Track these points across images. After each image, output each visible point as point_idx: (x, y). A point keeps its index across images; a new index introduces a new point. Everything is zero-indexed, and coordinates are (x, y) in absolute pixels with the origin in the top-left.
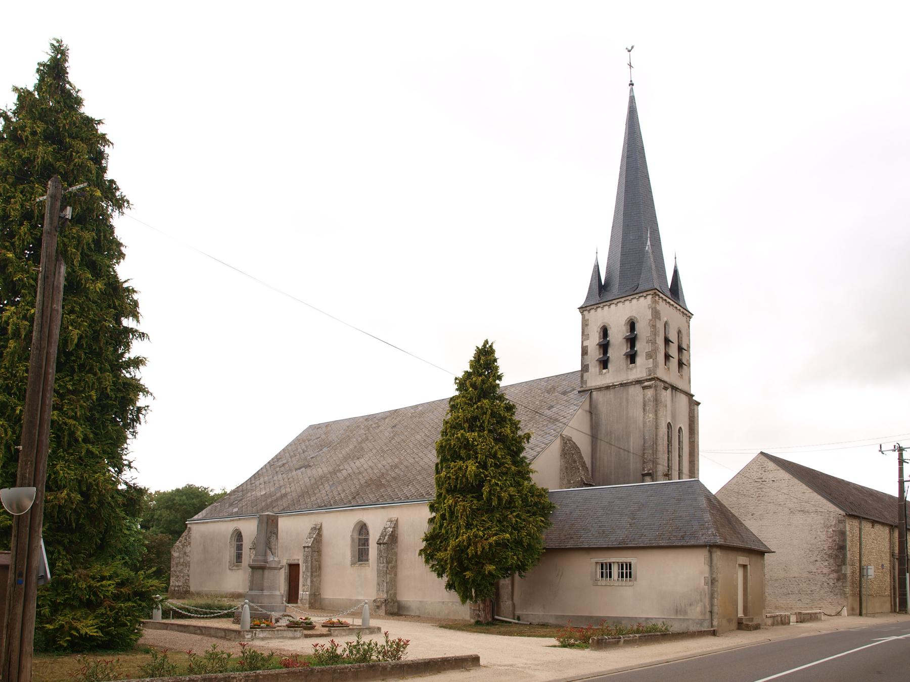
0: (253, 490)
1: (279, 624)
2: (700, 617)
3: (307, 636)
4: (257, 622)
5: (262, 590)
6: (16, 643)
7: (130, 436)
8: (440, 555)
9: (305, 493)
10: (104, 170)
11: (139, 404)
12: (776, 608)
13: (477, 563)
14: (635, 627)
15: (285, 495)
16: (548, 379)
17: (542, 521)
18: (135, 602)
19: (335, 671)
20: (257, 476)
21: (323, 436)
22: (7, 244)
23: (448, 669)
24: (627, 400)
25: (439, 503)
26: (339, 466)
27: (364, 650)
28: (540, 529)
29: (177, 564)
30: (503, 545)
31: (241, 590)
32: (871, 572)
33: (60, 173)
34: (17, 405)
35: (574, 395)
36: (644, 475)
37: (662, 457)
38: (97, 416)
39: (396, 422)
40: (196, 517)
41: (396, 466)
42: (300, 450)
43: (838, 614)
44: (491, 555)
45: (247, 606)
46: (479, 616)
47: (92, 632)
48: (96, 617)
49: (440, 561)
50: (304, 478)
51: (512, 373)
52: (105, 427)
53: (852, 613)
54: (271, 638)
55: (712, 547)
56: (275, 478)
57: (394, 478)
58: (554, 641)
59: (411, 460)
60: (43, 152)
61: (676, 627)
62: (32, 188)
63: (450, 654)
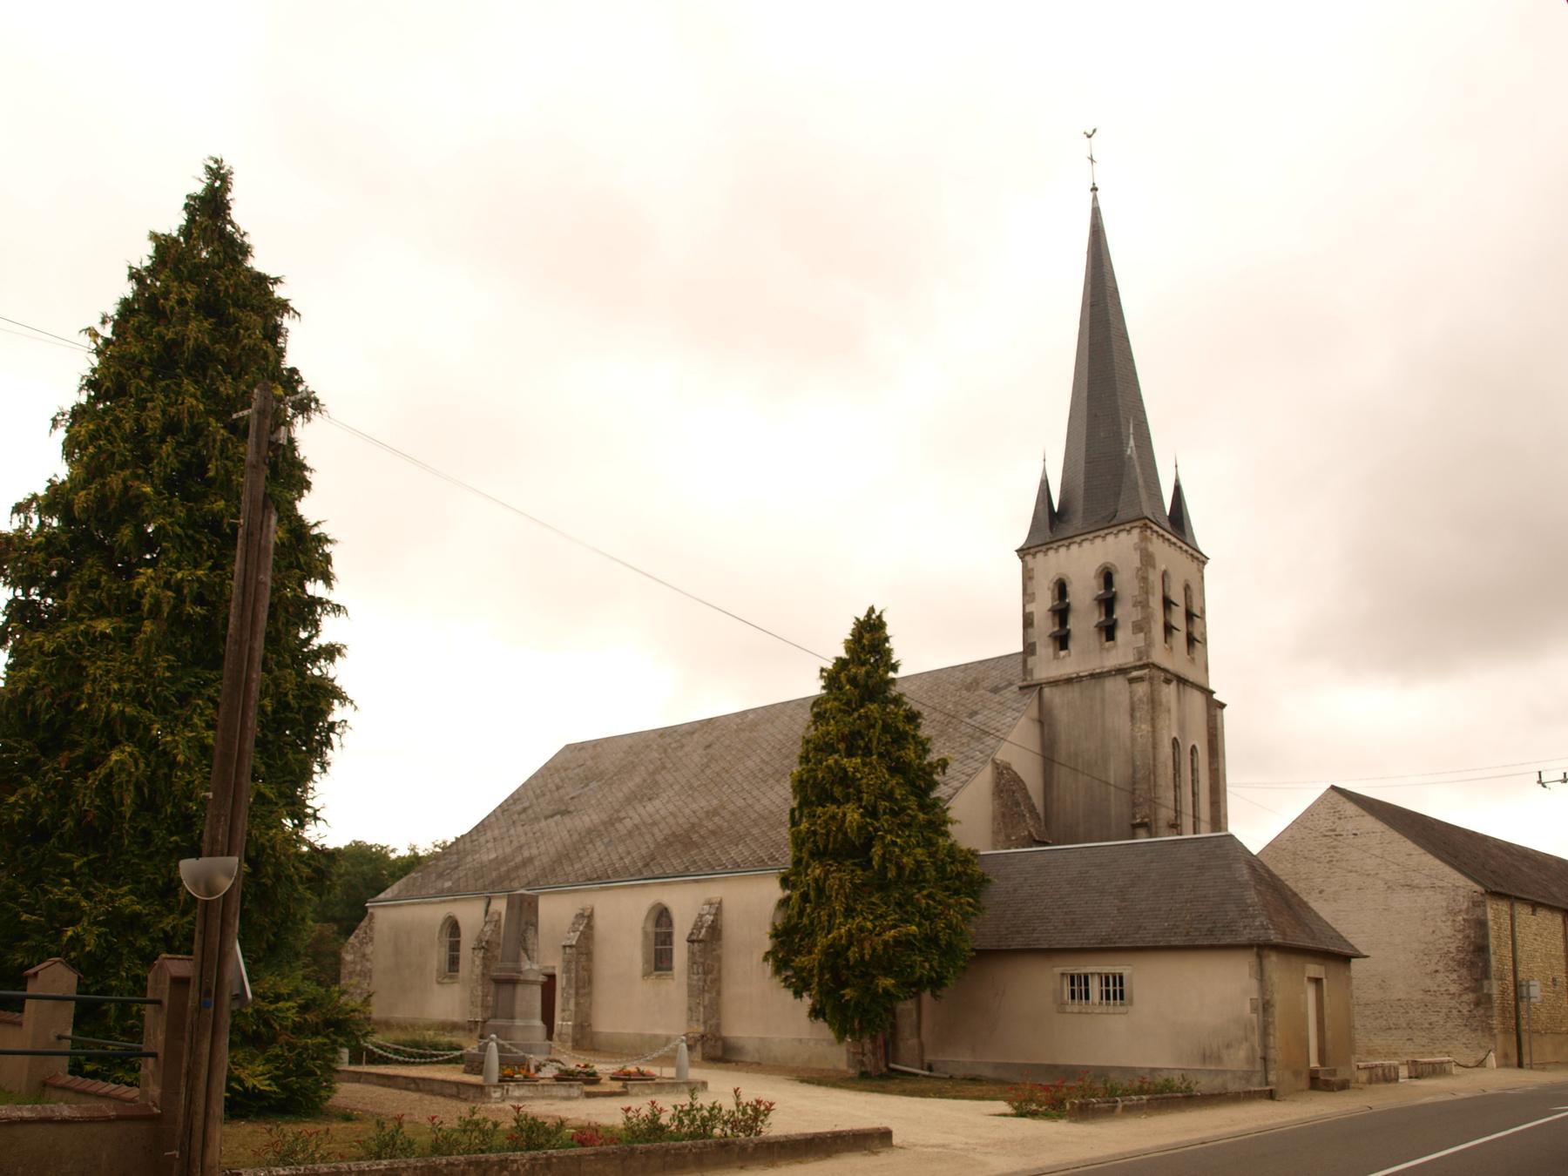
0: (476, 852)
1: (541, 1075)
2: (1246, 1068)
3: (589, 1095)
4: (508, 1071)
5: (513, 1018)
6: (201, 1102)
7: (316, 768)
8: (801, 961)
9: (563, 857)
10: (281, 353)
11: (331, 718)
12: (1369, 1053)
14: (1137, 1084)
15: (531, 860)
16: (966, 668)
17: (969, 904)
18: (327, 1036)
21: (589, 763)
22: (141, 471)
23: (843, 1151)
24: (1103, 700)
25: (798, 874)
27: (703, 1118)
28: (966, 917)
29: (351, 973)
30: (905, 943)
31: (456, 1017)
32: (1536, 991)
34: (153, 722)
35: (1011, 693)
36: (1135, 826)
39: (711, 738)
40: (382, 896)
41: (715, 812)
42: (551, 786)
43: (1481, 1064)
44: (887, 961)
45: (493, 1044)
46: (862, 1063)
47: (263, 1085)
48: (267, 1061)
49: (798, 972)
50: (559, 832)
51: (915, 655)
52: (283, 755)
53: (1504, 1063)
54: (532, 1098)
55: (1261, 948)
56: (512, 831)
57: (713, 833)
59: (740, 803)
60: (197, 330)
61: (1204, 1085)
62: (179, 385)
63: (845, 1126)
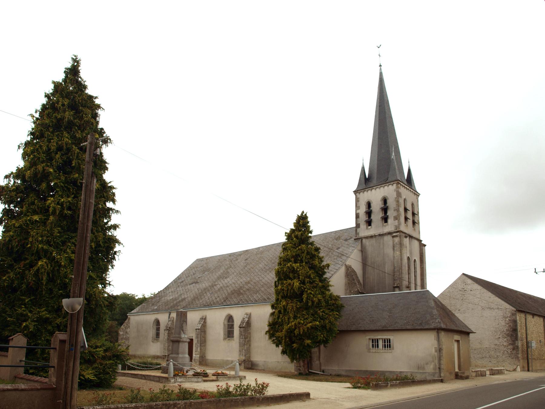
0: (165, 296)
1: (188, 374)
3: (205, 381)
4: (177, 373)
5: (178, 354)
6: (70, 383)
8: (278, 334)
9: (196, 298)
10: (97, 123)
11: (115, 250)
12: (476, 366)
13: (300, 339)
14: (395, 377)
15: (184, 299)
17: (337, 315)
18: (114, 360)
19: (232, 400)
20: (167, 288)
21: (205, 265)
23: (293, 400)
24: (383, 243)
25: (277, 304)
26: (215, 282)
27: (244, 389)
28: (336, 319)
30: (314, 328)
32: (534, 345)
33: (77, 126)
34: (53, 251)
35: (351, 241)
36: (394, 287)
37: (406, 277)
38: (94, 256)
39: (247, 257)
40: (133, 312)
41: (249, 283)
42: (192, 273)
43: (515, 370)
44: (308, 334)
45: (171, 363)
47: (91, 377)
48: (93, 369)
49: (278, 338)
50: (195, 289)
51: (318, 228)
52: (98, 262)
53: (523, 370)
54: (185, 382)
55: (438, 330)
56: (178, 289)
57: (248, 290)
58: (348, 385)
59: (257, 279)
60: (68, 115)
61: (418, 377)
62: (62, 134)
63: (294, 391)
